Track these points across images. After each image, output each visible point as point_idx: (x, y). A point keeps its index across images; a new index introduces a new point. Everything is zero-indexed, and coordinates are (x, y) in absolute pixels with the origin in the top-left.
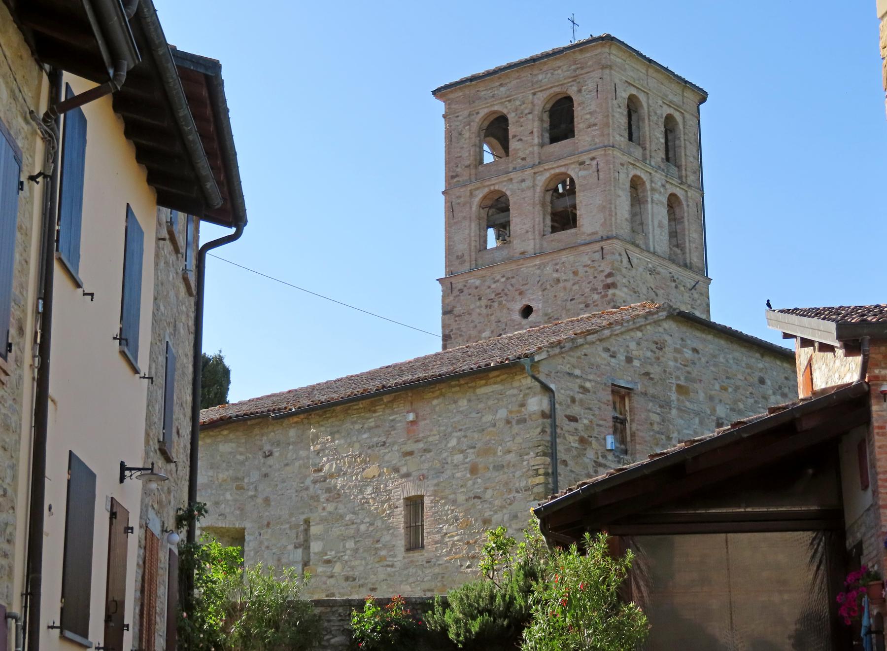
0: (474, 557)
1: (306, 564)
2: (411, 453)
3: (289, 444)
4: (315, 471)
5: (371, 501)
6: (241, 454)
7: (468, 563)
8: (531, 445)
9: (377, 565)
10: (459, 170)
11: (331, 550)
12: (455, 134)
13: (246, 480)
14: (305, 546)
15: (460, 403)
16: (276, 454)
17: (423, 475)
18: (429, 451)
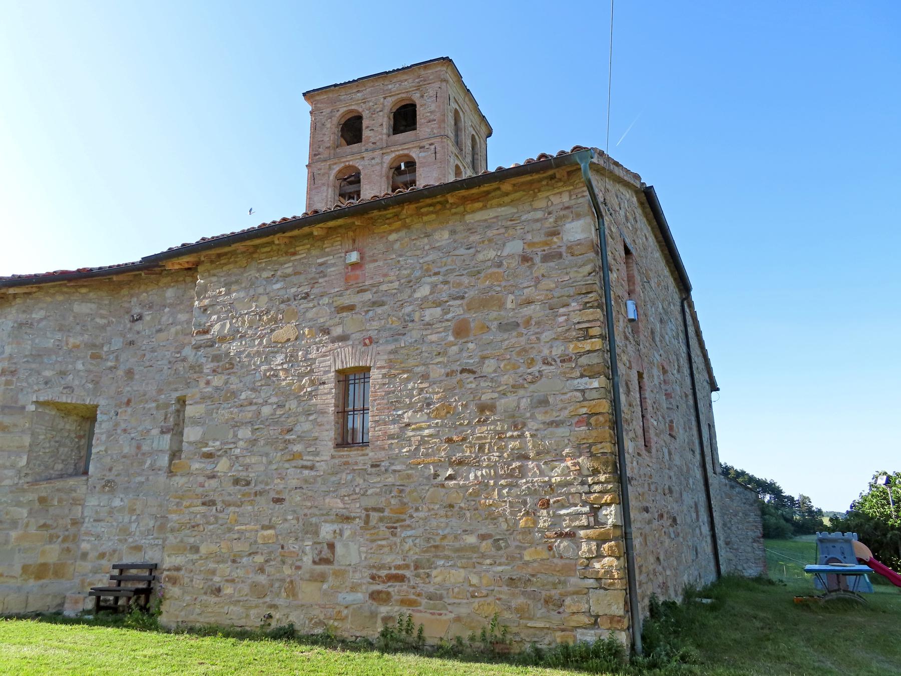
0: (460, 463)
1: (175, 454)
2: (351, 308)
3: (165, 306)
4: (198, 333)
5: (281, 373)
6: (102, 317)
7: (450, 472)
8: (572, 291)
9: (287, 465)
10: (320, 150)
11: (215, 440)
12: (318, 125)
13: (105, 349)
14: (177, 431)
15: (437, 236)
16: (148, 318)
17: (370, 338)
18: (382, 304)
